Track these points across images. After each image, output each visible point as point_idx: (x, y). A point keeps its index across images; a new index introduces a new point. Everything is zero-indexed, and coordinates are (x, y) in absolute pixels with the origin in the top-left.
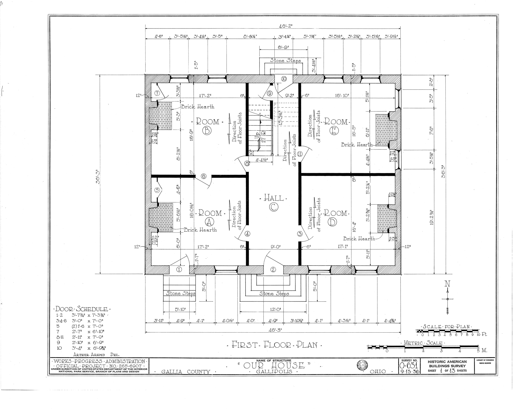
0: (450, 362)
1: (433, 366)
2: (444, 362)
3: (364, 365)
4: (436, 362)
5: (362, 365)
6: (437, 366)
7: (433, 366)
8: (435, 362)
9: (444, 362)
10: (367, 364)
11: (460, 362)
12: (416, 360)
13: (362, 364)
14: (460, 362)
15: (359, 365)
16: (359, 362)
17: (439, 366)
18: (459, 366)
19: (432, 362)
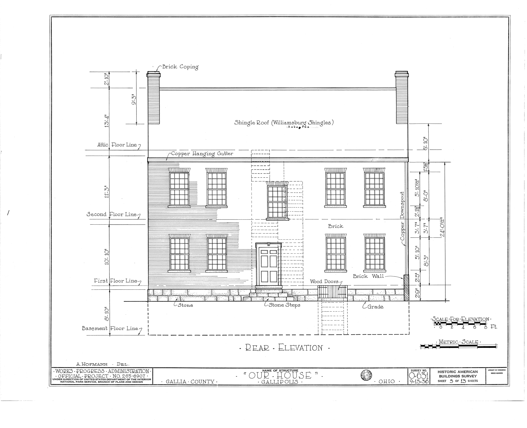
0: (460, 372)
1: (443, 376)
2: (455, 372)
3: (368, 375)
4: (446, 372)
5: (366, 375)
6: (447, 376)
7: (443, 376)
8: (445, 372)
9: (455, 372)
10: (371, 375)
11: (471, 372)
12: (425, 370)
13: (366, 374)
14: (471, 372)
15: (363, 375)
16: (363, 372)
17: (449, 376)
18: (469, 376)
19: (442, 372)
